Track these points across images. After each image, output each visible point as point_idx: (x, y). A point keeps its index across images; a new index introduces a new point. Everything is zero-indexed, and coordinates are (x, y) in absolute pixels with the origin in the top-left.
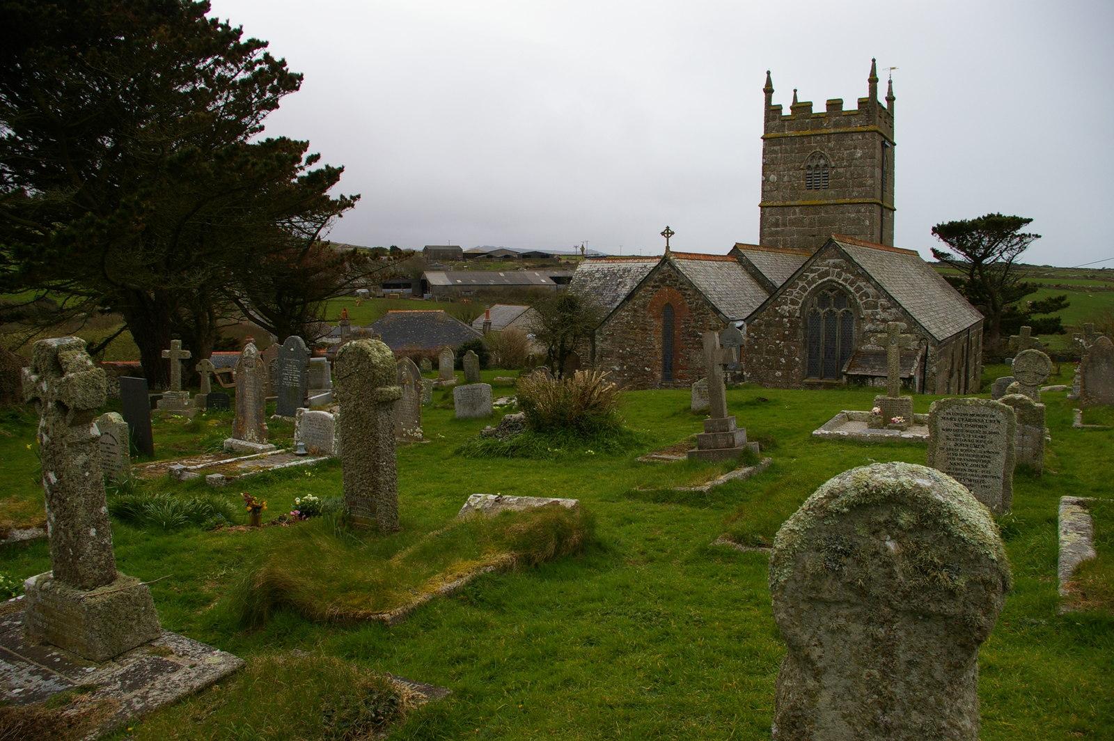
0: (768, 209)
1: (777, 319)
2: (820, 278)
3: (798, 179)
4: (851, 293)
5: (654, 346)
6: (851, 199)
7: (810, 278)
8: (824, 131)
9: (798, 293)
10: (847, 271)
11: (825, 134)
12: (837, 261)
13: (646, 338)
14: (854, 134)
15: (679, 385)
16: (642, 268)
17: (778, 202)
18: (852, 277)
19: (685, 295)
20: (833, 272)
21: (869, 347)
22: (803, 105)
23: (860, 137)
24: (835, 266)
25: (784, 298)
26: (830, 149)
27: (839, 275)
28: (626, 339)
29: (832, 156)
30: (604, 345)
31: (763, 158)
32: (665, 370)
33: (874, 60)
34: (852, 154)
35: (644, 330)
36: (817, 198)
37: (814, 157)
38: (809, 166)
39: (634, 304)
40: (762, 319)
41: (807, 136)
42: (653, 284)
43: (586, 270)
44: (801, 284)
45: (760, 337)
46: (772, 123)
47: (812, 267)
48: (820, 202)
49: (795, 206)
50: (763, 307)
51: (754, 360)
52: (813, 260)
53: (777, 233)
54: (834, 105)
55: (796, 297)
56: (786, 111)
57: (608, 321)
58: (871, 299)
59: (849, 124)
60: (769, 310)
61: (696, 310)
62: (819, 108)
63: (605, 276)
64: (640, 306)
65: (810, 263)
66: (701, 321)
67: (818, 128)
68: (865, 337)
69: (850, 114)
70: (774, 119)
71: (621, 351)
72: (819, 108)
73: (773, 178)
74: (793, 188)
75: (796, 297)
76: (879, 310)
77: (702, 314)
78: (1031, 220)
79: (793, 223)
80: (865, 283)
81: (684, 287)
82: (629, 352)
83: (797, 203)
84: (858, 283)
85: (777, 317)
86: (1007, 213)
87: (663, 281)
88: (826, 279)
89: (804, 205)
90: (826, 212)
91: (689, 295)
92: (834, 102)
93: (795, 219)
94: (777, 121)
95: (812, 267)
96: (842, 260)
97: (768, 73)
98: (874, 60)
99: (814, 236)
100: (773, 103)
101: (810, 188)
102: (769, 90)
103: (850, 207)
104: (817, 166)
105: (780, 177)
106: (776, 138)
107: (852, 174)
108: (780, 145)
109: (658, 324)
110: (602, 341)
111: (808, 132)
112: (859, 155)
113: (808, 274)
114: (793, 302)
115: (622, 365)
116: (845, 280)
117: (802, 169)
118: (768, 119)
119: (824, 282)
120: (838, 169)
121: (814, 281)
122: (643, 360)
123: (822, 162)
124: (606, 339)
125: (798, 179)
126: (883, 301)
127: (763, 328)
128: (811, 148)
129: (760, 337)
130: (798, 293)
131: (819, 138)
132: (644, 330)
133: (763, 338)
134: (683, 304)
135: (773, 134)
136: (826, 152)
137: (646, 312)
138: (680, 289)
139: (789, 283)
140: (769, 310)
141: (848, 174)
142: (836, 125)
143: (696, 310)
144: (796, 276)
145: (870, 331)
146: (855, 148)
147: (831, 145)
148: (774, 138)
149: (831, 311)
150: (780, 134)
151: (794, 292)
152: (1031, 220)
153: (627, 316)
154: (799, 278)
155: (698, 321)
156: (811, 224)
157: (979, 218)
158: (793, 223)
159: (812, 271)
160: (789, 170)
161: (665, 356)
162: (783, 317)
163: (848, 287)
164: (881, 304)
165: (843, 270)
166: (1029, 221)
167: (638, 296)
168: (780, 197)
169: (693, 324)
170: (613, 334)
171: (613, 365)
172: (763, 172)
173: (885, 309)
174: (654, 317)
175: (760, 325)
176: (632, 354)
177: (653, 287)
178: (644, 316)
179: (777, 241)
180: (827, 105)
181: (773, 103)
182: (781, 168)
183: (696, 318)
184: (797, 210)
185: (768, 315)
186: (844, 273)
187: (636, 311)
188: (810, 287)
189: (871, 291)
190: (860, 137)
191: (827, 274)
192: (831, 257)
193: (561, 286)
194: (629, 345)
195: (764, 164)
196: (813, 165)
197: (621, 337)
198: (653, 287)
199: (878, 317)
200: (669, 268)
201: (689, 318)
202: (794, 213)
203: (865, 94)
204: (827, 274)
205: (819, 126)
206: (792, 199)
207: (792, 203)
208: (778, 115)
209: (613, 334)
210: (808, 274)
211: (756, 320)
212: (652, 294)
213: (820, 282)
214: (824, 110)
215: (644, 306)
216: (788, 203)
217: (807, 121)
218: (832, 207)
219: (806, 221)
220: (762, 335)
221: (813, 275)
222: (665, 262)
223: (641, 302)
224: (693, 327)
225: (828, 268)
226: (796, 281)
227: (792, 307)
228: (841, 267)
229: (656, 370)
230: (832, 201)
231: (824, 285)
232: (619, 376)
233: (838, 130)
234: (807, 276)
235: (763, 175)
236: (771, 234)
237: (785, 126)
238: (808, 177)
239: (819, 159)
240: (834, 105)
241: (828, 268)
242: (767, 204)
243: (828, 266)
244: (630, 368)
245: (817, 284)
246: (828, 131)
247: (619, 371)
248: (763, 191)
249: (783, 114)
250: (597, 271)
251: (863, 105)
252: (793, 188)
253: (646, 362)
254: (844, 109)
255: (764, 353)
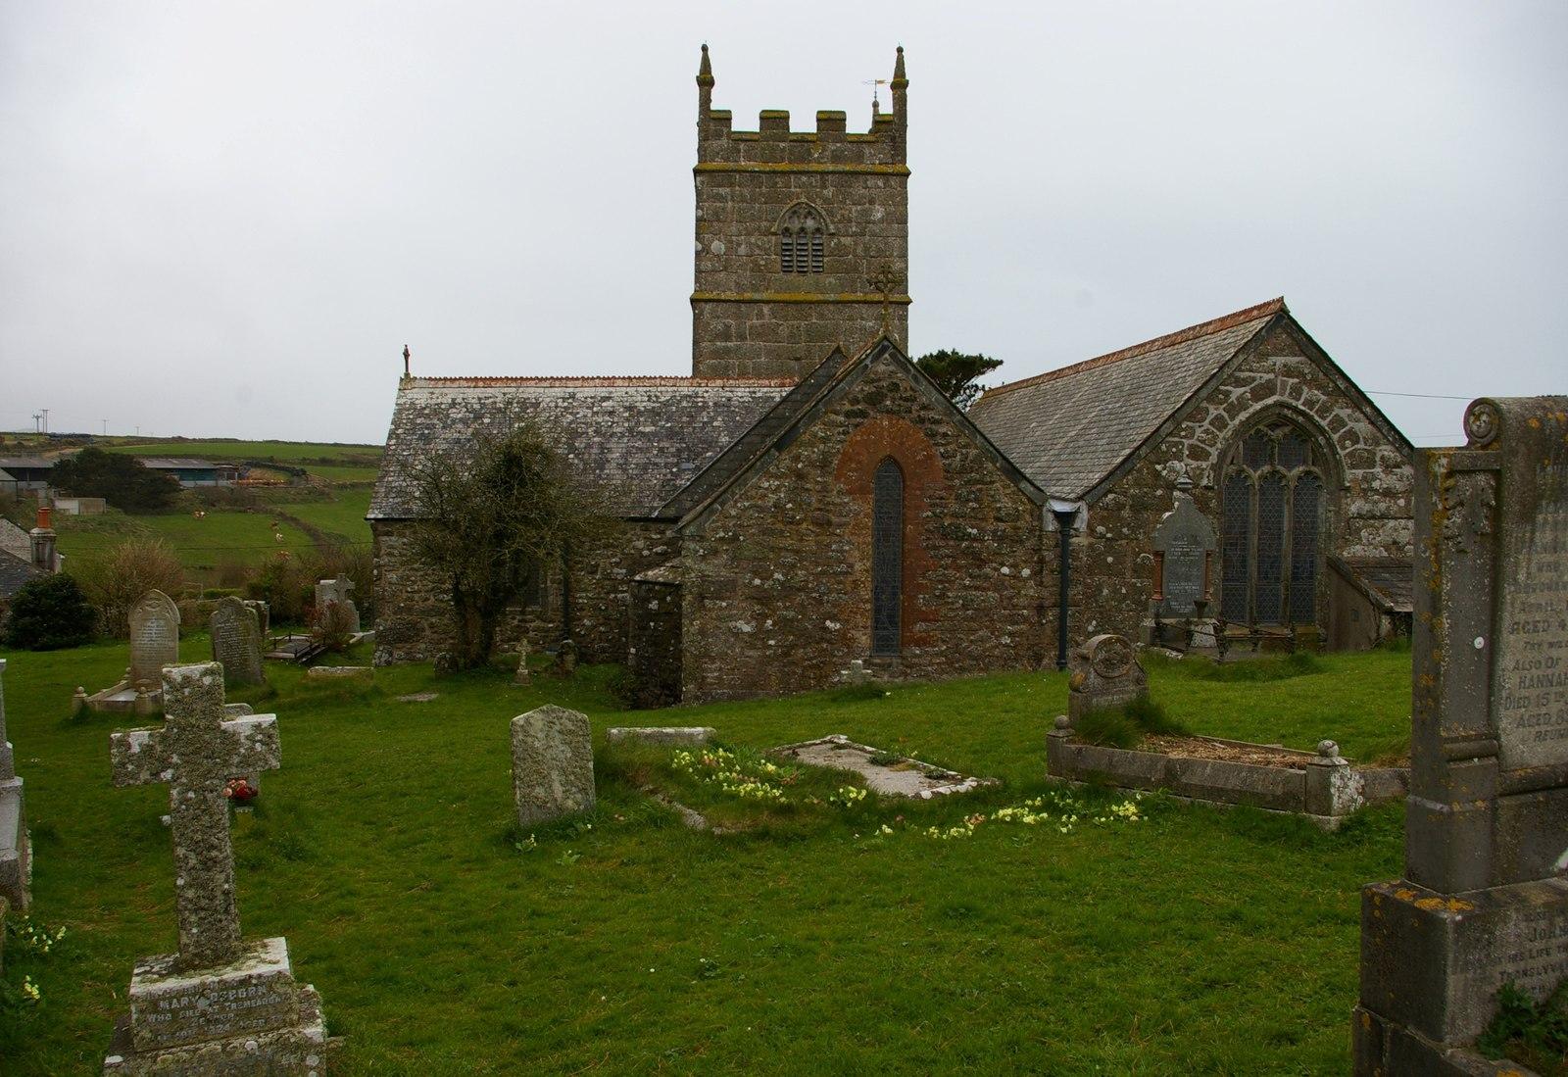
0: (708, 307)
1: (1159, 492)
2: (1257, 398)
3: (767, 252)
4: (1322, 431)
5: (851, 566)
6: (866, 294)
7: (1233, 398)
8: (814, 167)
9: (1207, 431)
10: (1314, 383)
11: (817, 172)
12: (1293, 360)
13: (828, 546)
14: (869, 177)
15: (916, 660)
16: (564, 399)
17: (728, 293)
18: (1324, 398)
19: (933, 435)
20: (1284, 384)
21: (1357, 550)
22: (776, 115)
23: (880, 184)
24: (1288, 372)
25: (1176, 444)
26: (826, 200)
27: (1296, 392)
28: (772, 549)
29: (831, 214)
30: (708, 569)
31: (697, 208)
32: (877, 625)
33: (900, 50)
34: (866, 213)
35: (824, 524)
36: (803, 288)
37: (795, 212)
38: (787, 229)
39: (797, 458)
40: (1125, 494)
41: (783, 173)
42: (848, 407)
43: (421, 402)
44: (1213, 412)
45: (1120, 536)
46: (715, 144)
47: (1237, 374)
48: (809, 297)
49: (763, 302)
50: (1128, 466)
51: (1105, 591)
52: (1241, 357)
53: (727, 351)
54: (831, 122)
55: (1203, 442)
56: (746, 122)
57: (722, 504)
58: (1361, 445)
59: (859, 158)
60: (1139, 471)
61: (963, 471)
62: (803, 123)
63: (478, 417)
64: (812, 464)
65: (1236, 362)
66: (976, 500)
67: (802, 160)
68: (1350, 530)
69: (859, 140)
70: (719, 136)
71: (757, 582)
72: (803, 123)
73: (718, 246)
74: (756, 268)
75: (1203, 442)
76: (1378, 470)
77: (978, 482)
78: (1001, 362)
79: (759, 334)
80: (1349, 411)
81: (931, 414)
82: (782, 584)
83: (765, 296)
84: (1336, 411)
85: (1156, 487)
86: (966, 351)
87: (874, 399)
88: (1270, 401)
89: (779, 302)
90: (822, 316)
91: (945, 435)
92: (833, 116)
93: (762, 325)
94: (724, 141)
95: (1237, 374)
96: (1302, 358)
97: (705, 49)
98: (900, 50)
99: (797, 359)
100: (713, 107)
101: (787, 269)
102: (706, 82)
103: (864, 309)
104: (803, 229)
105: (732, 247)
106: (723, 171)
107: (866, 249)
108: (731, 185)
109: (862, 508)
110: (704, 557)
111: (783, 166)
112: (879, 215)
113: (1229, 388)
114: (1197, 453)
115: (760, 618)
116: (1310, 403)
117: (775, 234)
118: (705, 135)
119: (1267, 408)
120: (842, 239)
121: (1242, 405)
122: (819, 602)
123: (810, 223)
124: (715, 553)
125: (767, 252)
126: (1386, 450)
127: (1126, 513)
128: (790, 196)
129: (1120, 536)
130: (1207, 431)
131: (804, 178)
132: (824, 524)
133: (1127, 537)
134: (930, 457)
135: (717, 164)
136: (818, 205)
137: (830, 479)
138: (922, 420)
139: (1188, 409)
140: (1139, 471)
141: (860, 250)
142: (836, 158)
143: (963, 471)
144: (1204, 393)
145: (1360, 516)
146: (872, 202)
147: (829, 192)
148: (719, 171)
149: (1274, 473)
150: (731, 165)
151: (1198, 431)
152: (1001, 362)
153: (778, 489)
154: (1210, 399)
155: (968, 501)
156: (793, 337)
157: (925, 357)
158: (759, 334)
159: (1239, 383)
160: (749, 234)
161: (877, 593)
162: (1171, 486)
163: (1317, 418)
164: (1382, 457)
165: (1305, 382)
166: (993, 364)
167: (806, 437)
168: (733, 285)
169: (954, 507)
170: (735, 538)
171: (731, 618)
172: (697, 234)
173: (1389, 467)
174: (850, 492)
175: (1120, 507)
176: (788, 590)
177: (848, 415)
178: (825, 489)
179: (726, 368)
180: (818, 120)
181: (713, 107)
182: (734, 229)
183: (964, 492)
184: (766, 309)
185: (1137, 484)
186: (1305, 389)
187: (800, 476)
188: (1232, 418)
189: (1363, 427)
190: (880, 184)
191: (1269, 389)
192: (1279, 351)
193: (22, 484)
194: (780, 566)
195: (699, 220)
196: (795, 225)
197: (758, 543)
198: (848, 415)
199: (1376, 484)
200: (892, 368)
201: (943, 493)
202: (760, 315)
203: (887, 108)
204: (1269, 389)
205: (805, 158)
206: (755, 289)
207: (757, 296)
208: (725, 130)
209: (735, 538)
210: (1229, 388)
211: (1111, 496)
212: (844, 433)
213: (1258, 406)
214: (811, 127)
215: (824, 465)
216: (748, 296)
217: (782, 145)
218: (831, 307)
219: (784, 331)
220: (1125, 530)
221: (1243, 389)
222: (884, 350)
223: (816, 453)
224: (955, 515)
225: (1272, 376)
226: (1204, 404)
227: (1194, 464)
228: (1301, 375)
229: (856, 627)
230: (832, 297)
231: (1265, 414)
232: (752, 647)
233: (840, 167)
234: (1227, 394)
235: (697, 239)
236: (717, 354)
237: (739, 151)
238: (786, 249)
239: (806, 218)
240: (831, 122)
241: (1272, 376)
242: (707, 296)
243: (1273, 371)
244: (784, 625)
245: (1251, 410)
246: (822, 167)
247: (750, 635)
248: (698, 271)
249: (733, 130)
250: (453, 404)
251: (883, 127)
252: (756, 268)
253: (828, 607)
254: (848, 130)
255: (1128, 574)
